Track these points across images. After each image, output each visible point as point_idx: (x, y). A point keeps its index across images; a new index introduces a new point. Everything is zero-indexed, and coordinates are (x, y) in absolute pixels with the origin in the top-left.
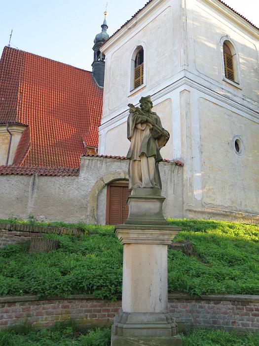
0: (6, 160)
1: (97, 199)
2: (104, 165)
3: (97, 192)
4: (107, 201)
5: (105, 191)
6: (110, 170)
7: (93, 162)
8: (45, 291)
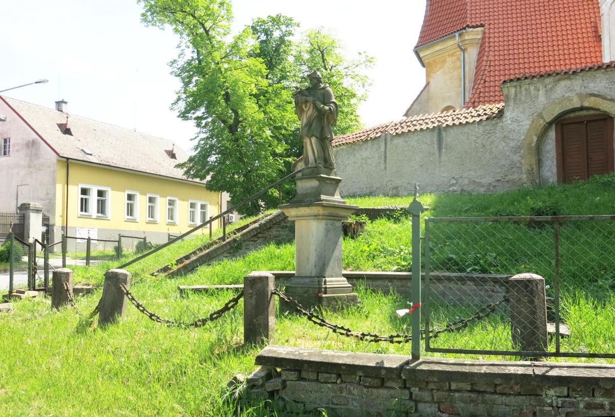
0: (45, 139)
1: (538, 150)
2: (542, 92)
3: (535, 139)
4: (557, 151)
5: (552, 134)
6: (553, 97)
7: (523, 89)
8: (176, 249)
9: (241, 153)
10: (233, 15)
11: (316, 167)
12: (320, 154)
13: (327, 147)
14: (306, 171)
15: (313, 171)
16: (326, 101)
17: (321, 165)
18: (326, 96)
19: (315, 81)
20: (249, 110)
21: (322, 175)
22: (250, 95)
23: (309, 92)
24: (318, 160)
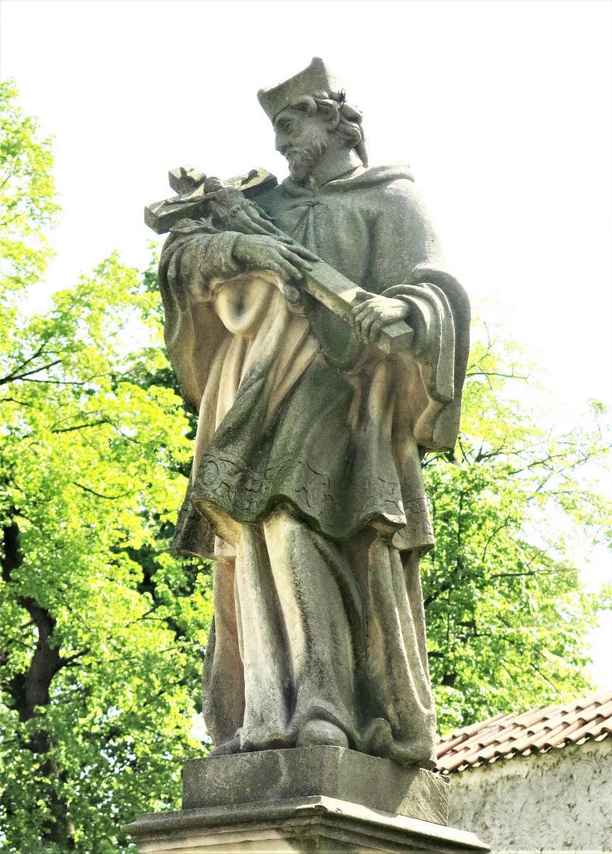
9: (57, 803)
10: (55, 201)
11: (291, 743)
12: (324, 650)
13: (381, 602)
14: (218, 777)
15: (267, 775)
16: (384, 266)
17: (326, 729)
18: (386, 237)
19: (313, 132)
20: (102, 610)
21: (331, 804)
22: (115, 550)
23: (268, 212)
24: (303, 690)
